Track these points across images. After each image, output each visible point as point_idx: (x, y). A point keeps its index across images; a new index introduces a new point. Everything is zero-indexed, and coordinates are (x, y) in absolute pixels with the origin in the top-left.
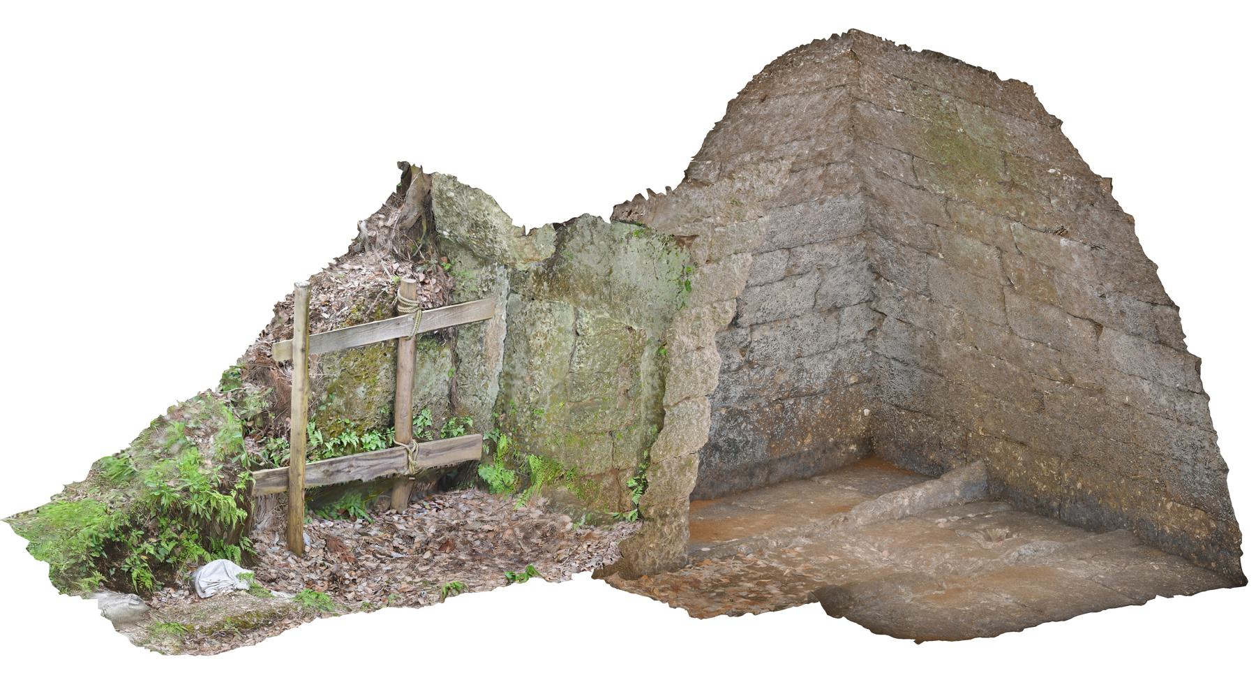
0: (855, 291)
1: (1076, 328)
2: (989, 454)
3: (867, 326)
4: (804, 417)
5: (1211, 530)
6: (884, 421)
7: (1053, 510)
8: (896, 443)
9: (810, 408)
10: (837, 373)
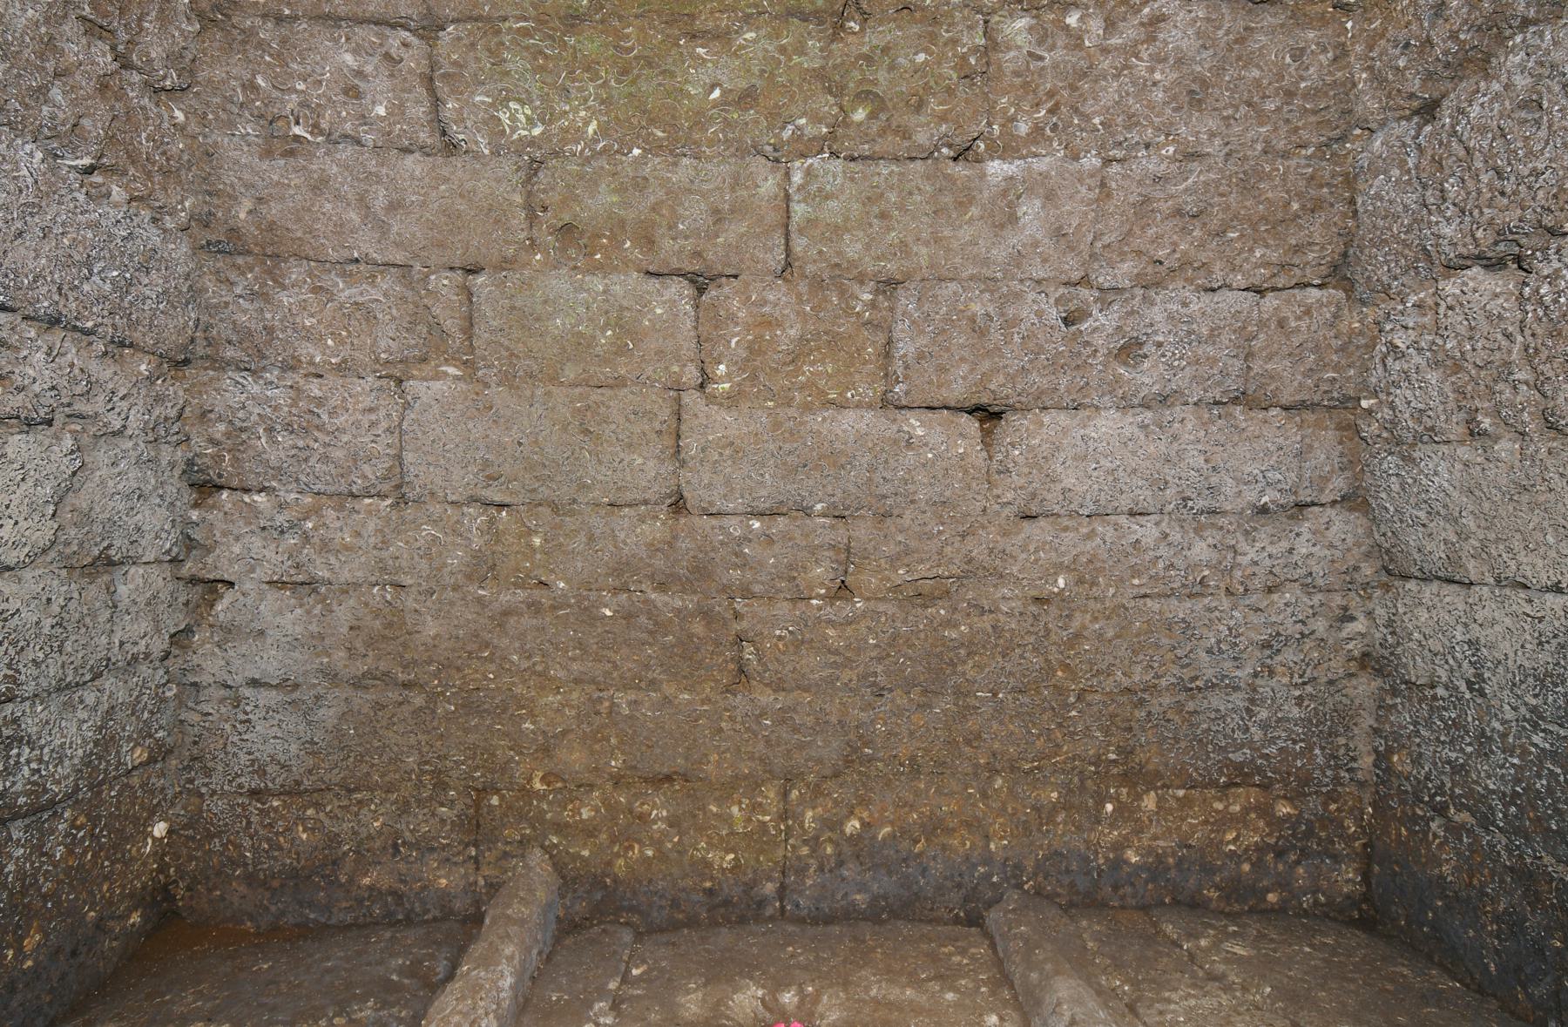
0: (154, 525)
1: (937, 437)
2: (560, 828)
3: (175, 620)
4: (21, 874)
5: (1275, 823)
6: (210, 836)
7: (762, 903)
8: (250, 879)
9: (39, 849)
10: (106, 742)
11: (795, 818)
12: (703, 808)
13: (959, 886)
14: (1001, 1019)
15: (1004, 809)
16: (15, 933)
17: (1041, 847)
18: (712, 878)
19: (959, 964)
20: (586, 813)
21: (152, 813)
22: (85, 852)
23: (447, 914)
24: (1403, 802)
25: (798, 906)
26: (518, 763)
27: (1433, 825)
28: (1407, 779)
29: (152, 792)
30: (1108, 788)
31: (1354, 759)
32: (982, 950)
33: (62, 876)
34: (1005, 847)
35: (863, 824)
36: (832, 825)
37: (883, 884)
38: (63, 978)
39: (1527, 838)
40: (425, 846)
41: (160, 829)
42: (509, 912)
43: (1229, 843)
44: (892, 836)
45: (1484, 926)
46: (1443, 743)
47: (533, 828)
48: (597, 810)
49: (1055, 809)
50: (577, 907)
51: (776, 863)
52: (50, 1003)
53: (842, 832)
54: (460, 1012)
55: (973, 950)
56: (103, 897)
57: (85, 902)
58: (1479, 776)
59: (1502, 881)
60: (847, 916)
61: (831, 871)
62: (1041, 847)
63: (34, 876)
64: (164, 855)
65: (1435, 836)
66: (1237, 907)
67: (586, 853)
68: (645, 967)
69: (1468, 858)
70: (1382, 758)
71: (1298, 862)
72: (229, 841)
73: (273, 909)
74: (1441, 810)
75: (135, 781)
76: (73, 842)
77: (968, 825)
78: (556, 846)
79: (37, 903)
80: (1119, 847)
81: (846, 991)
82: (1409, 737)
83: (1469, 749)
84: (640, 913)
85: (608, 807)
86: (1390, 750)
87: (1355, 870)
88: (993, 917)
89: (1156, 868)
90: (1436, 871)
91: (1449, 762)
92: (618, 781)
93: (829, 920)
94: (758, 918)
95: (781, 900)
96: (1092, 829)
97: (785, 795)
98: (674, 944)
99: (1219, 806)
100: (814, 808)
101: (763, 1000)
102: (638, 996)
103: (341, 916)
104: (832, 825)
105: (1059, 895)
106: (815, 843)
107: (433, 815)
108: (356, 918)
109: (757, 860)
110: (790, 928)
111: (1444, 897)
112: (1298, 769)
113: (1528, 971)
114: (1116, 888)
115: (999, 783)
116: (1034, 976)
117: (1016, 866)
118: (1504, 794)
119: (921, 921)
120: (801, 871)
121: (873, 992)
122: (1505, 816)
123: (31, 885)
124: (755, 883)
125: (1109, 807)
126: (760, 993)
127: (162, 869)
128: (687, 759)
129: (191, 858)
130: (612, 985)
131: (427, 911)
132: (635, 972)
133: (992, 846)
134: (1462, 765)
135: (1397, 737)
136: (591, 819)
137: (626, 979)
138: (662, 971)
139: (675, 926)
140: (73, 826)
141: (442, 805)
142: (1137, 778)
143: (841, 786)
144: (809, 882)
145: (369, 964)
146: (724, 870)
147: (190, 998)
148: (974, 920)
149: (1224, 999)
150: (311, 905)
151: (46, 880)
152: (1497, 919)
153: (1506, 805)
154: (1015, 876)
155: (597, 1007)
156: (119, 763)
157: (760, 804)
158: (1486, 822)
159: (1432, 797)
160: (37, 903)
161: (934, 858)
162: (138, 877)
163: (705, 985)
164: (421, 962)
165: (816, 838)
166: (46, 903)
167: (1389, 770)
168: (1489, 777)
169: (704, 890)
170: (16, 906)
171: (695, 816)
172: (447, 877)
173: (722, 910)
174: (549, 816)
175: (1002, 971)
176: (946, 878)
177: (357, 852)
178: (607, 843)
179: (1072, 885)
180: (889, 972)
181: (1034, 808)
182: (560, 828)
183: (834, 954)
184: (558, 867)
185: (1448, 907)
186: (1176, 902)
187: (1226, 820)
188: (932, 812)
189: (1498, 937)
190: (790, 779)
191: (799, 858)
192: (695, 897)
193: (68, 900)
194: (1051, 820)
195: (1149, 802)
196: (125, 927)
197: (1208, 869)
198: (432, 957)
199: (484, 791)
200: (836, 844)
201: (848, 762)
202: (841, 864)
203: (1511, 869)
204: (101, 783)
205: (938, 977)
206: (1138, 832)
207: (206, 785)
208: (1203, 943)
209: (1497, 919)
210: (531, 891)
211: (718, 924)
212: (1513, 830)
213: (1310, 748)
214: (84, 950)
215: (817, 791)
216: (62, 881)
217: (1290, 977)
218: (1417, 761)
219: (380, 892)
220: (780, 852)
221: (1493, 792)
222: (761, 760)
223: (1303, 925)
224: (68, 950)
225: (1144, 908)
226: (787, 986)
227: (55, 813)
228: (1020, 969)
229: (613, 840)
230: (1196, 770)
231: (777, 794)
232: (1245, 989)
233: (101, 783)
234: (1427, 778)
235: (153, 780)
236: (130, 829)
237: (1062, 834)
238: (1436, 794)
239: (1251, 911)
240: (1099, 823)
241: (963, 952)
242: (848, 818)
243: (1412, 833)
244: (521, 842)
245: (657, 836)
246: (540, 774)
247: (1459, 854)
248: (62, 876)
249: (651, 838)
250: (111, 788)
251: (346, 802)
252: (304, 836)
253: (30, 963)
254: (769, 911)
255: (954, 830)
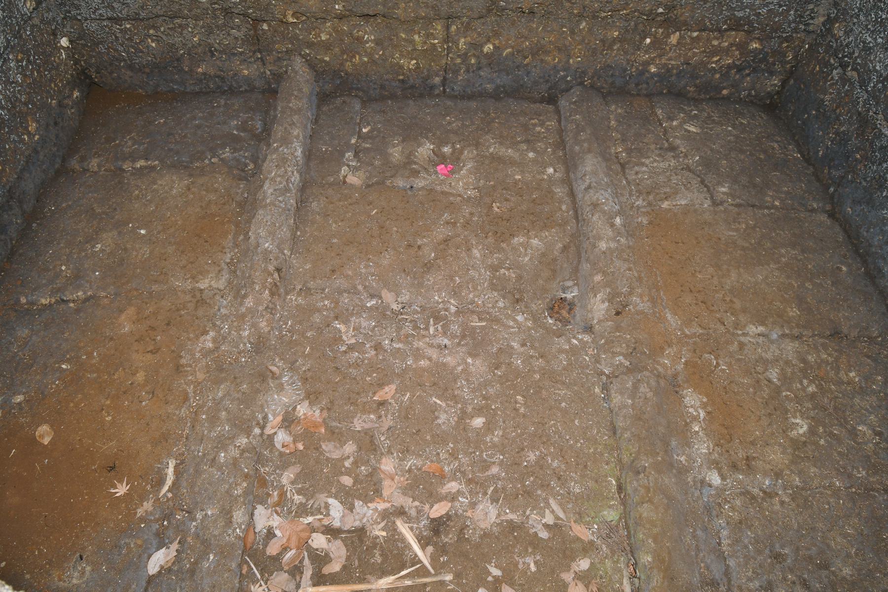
2: (310, 45)
6: (97, 44)
7: (432, 87)
8: (131, 67)
11: (454, 42)
12: (397, 35)
13: (547, 81)
14: (555, 171)
15: (583, 40)
16: (22, 126)
17: (600, 63)
18: (403, 74)
19: (539, 133)
20: (324, 37)
21: (54, 34)
22: (32, 73)
23: (252, 89)
24: (826, 52)
25: (453, 89)
26: (275, 6)
27: (835, 72)
28: (836, 40)
29: (49, 23)
30: (651, 28)
31: (812, 18)
32: (552, 124)
33: (28, 90)
34: (579, 62)
35: (495, 47)
36: (476, 46)
37: (504, 80)
38: (57, 136)
39: (877, 103)
40: (231, 53)
41: (64, 42)
42: (291, 105)
43: (713, 63)
44: (512, 54)
45: (828, 134)
46: (869, 29)
47: (293, 44)
48: (331, 35)
49: (614, 41)
50: (326, 87)
51: (441, 67)
52: (58, 150)
53: (482, 51)
54: (279, 176)
55: (548, 123)
56: (54, 91)
57: (47, 98)
58: (874, 59)
59: (851, 117)
60: (481, 95)
61: (473, 72)
62: (600, 63)
63: (14, 96)
64: (74, 54)
65: (832, 79)
66: (703, 96)
67: (327, 59)
68: (369, 127)
69: (842, 97)
70: (830, 21)
71: (748, 75)
72: (109, 47)
73: (151, 83)
74: (844, 66)
75: (36, 21)
76: (23, 70)
77: (559, 49)
78: (309, 55)
79: (24, 109)
80: (647, 63)
81: (477, 149)
82: (852, 16)
83: (880, 40)
84: (363, 91)
85: (337, 31)
86: (836, 19)
87: (780, 80)
88: (563, 103)
89: (665, 74)
90: (822, 96)
91: (864, 42)
92: (341, 17)
93: (470, 97)
94: (431, 95)
95: (444, 86)
96: (633, 54)
97: (448, 28)
98: (384, 112)
99: (715, 43)
100: (465, 37)
101: (433, 150)
102: (368, 148)
103: (192, 88)
104: (476, 46)
105: (603, 88)
106: (465, 57)
107: (229, 35)
108: (201, 89)
109: (430, 65)
110: (449, 103)
111: (817, 110)
112: (775, 23)
113: (836, 163)
114: (637, 85)
115: (583, 25)
116: (577, 148)
117: (583, 72)
118: (881, 75)
119: (522, 98)
120: (456, 72)
121: (491, 150)
122: (874, 87)
123: (15, 101)
124: (428, 77)
125: (648, 41)
126: (432, 147)
127: (77, 62)
128: (384, 6)
129: (91, 57)
130: (353, 141)
131: (241, 87)
132: (364, 130)
133: (571, 61)
134: (870, 48)
135: (845, 12)
136: (327, 40)
137: (360, 136)
138: (379, 131)
139: (382, 98)
140: (18, 61)
141: (233, 29)
142: (670, 23)
143: (483, 24)
144: (460, 78)
145: (219, 124)
146: (410, 69)
147: (130, 143)
148: (552, 100)
149: (673, 162)
150: (172, 81)
151: (21, 95)
152: (837, 133)
153: (878, 82)
154: (580, 77)
155: (347, 155)
156: (22, 15)
157: (432, 34)
158: (863, 84)
159: (844, 57)
160: (24, 109)
161: (535, 67)
162: (66, 73)
163: (403, 141)
164: (246, 122)
165: (466, 54)
166: (27, 106)
167: (829, 31)
168: (880, 62)
169: (399, 80)
170: (15, 114)
171: (391, 40)
172: (248, 70)
173: (410, 91)
174: (301, 37)
175: (561, 137)
176: (540, 78)
177: (189, 54)
178: (339, 53)
179: (613, 83)
180: (501, 137)
181: (602, 41)
182: (310, 45)
183: (473, 123)
184: (311, 65)
185: (816, 117)
186: (669, 92)
187: (716, 51)
188: (538, 41)
189: (832, 142)
190: (450, 18)
191: (455, 64)
192: (394, 84)
193: (38, 100)
194: (610, 48)
195: (674, 39)
196: (73, 101)
197: (694, 77)
198: (252, 119)
199: (257, 21)
200: (478, 57)
201: (489, 11)
202: (480, 68)
203: (860, 114)
204: (19, 32)
205: (527, 141)
206: (660, 56)
207: (79, 14)
208: (675, 123)
209: (837, 133)
210: (300, 90)
211: (407, 97)
212: (873, 95)
213: (788, 11)
214: (60, 120)
215: (467, 27)
216: (30, 92)
217: (712, 150)
218: (847, 33)
219: (210, 76)
220: (444, 62)
221: (877, 71)
222: (433, 7)
223: (735, 109)
224: (52, 123)
225: (649, 96)
226: (447, 143)
227: (5, 59)
228: (571, 141)
229: (343, 52)
230: (710, 21)
231: (442, 27)
232: (686, 156)
233: (19, 32)
234: (847, 46)
235: (46, 15)
236: (49, 49)
237: (616, 56)
238: (846, 56)
239: (710, 98)
240: (639, 49)
241: (542, 124)
242: (486, 43)
243: (821, 71)
244: (287, 52)
245: (369, 50)
246: (291, 12)
247: (839, 93)
248: (28, 90)
249: (366, 52)
250: (26, 31)
251: (171, 26)
252: (154, 45)
253: (37, 137)
254: (437, 92)
255: (550, 52)
